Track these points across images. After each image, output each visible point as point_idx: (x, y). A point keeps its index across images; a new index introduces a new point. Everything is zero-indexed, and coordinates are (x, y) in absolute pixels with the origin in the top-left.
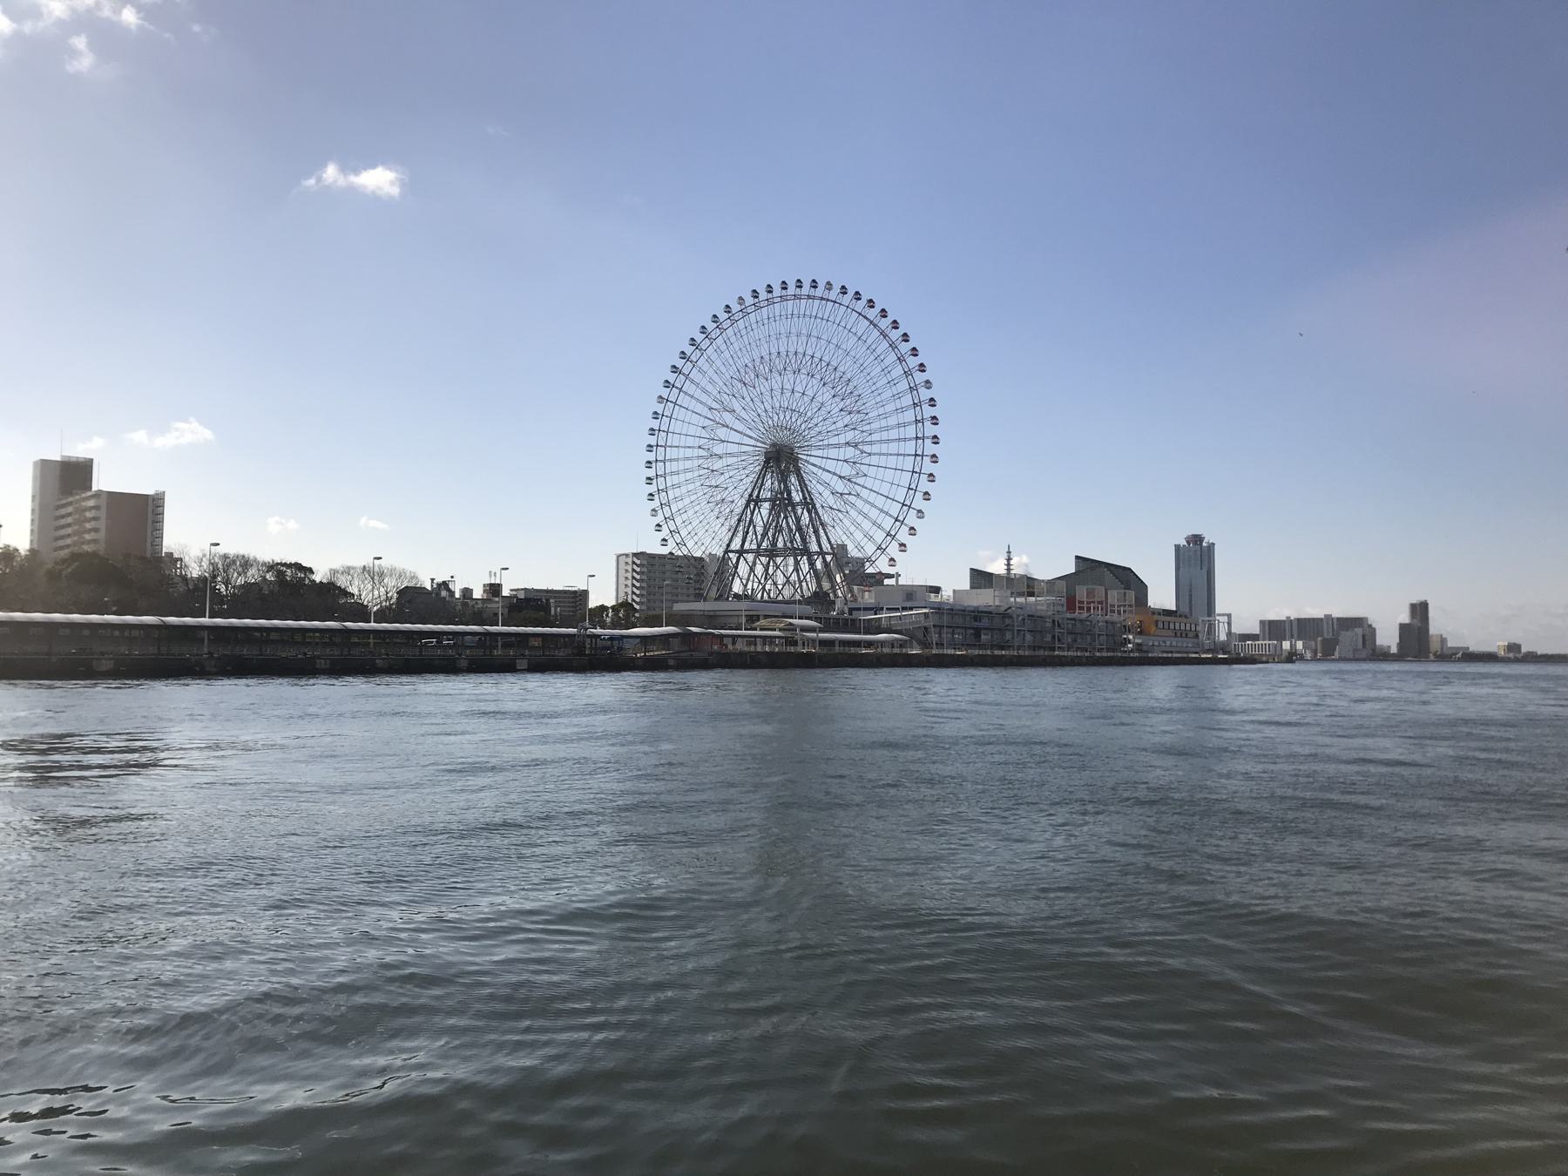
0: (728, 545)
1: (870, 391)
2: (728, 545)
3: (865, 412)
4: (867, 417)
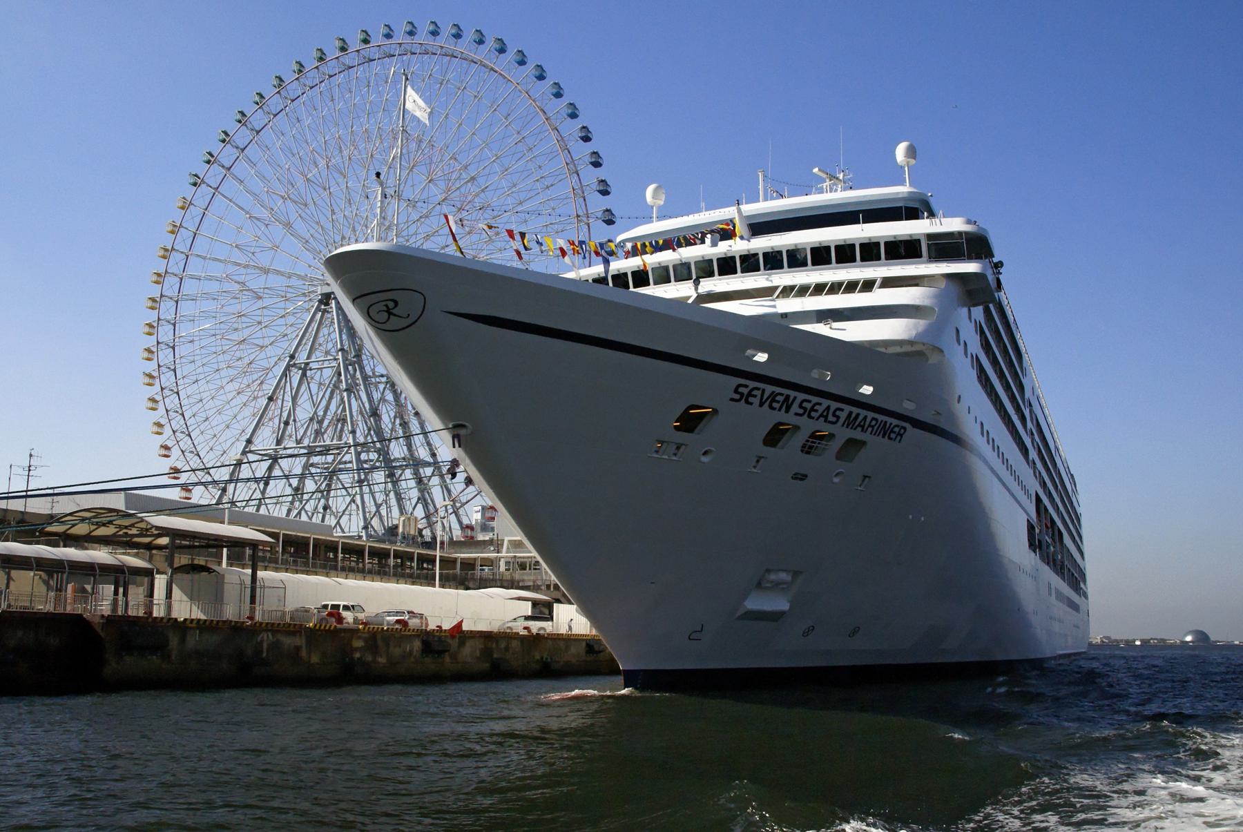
2: (249, 441)
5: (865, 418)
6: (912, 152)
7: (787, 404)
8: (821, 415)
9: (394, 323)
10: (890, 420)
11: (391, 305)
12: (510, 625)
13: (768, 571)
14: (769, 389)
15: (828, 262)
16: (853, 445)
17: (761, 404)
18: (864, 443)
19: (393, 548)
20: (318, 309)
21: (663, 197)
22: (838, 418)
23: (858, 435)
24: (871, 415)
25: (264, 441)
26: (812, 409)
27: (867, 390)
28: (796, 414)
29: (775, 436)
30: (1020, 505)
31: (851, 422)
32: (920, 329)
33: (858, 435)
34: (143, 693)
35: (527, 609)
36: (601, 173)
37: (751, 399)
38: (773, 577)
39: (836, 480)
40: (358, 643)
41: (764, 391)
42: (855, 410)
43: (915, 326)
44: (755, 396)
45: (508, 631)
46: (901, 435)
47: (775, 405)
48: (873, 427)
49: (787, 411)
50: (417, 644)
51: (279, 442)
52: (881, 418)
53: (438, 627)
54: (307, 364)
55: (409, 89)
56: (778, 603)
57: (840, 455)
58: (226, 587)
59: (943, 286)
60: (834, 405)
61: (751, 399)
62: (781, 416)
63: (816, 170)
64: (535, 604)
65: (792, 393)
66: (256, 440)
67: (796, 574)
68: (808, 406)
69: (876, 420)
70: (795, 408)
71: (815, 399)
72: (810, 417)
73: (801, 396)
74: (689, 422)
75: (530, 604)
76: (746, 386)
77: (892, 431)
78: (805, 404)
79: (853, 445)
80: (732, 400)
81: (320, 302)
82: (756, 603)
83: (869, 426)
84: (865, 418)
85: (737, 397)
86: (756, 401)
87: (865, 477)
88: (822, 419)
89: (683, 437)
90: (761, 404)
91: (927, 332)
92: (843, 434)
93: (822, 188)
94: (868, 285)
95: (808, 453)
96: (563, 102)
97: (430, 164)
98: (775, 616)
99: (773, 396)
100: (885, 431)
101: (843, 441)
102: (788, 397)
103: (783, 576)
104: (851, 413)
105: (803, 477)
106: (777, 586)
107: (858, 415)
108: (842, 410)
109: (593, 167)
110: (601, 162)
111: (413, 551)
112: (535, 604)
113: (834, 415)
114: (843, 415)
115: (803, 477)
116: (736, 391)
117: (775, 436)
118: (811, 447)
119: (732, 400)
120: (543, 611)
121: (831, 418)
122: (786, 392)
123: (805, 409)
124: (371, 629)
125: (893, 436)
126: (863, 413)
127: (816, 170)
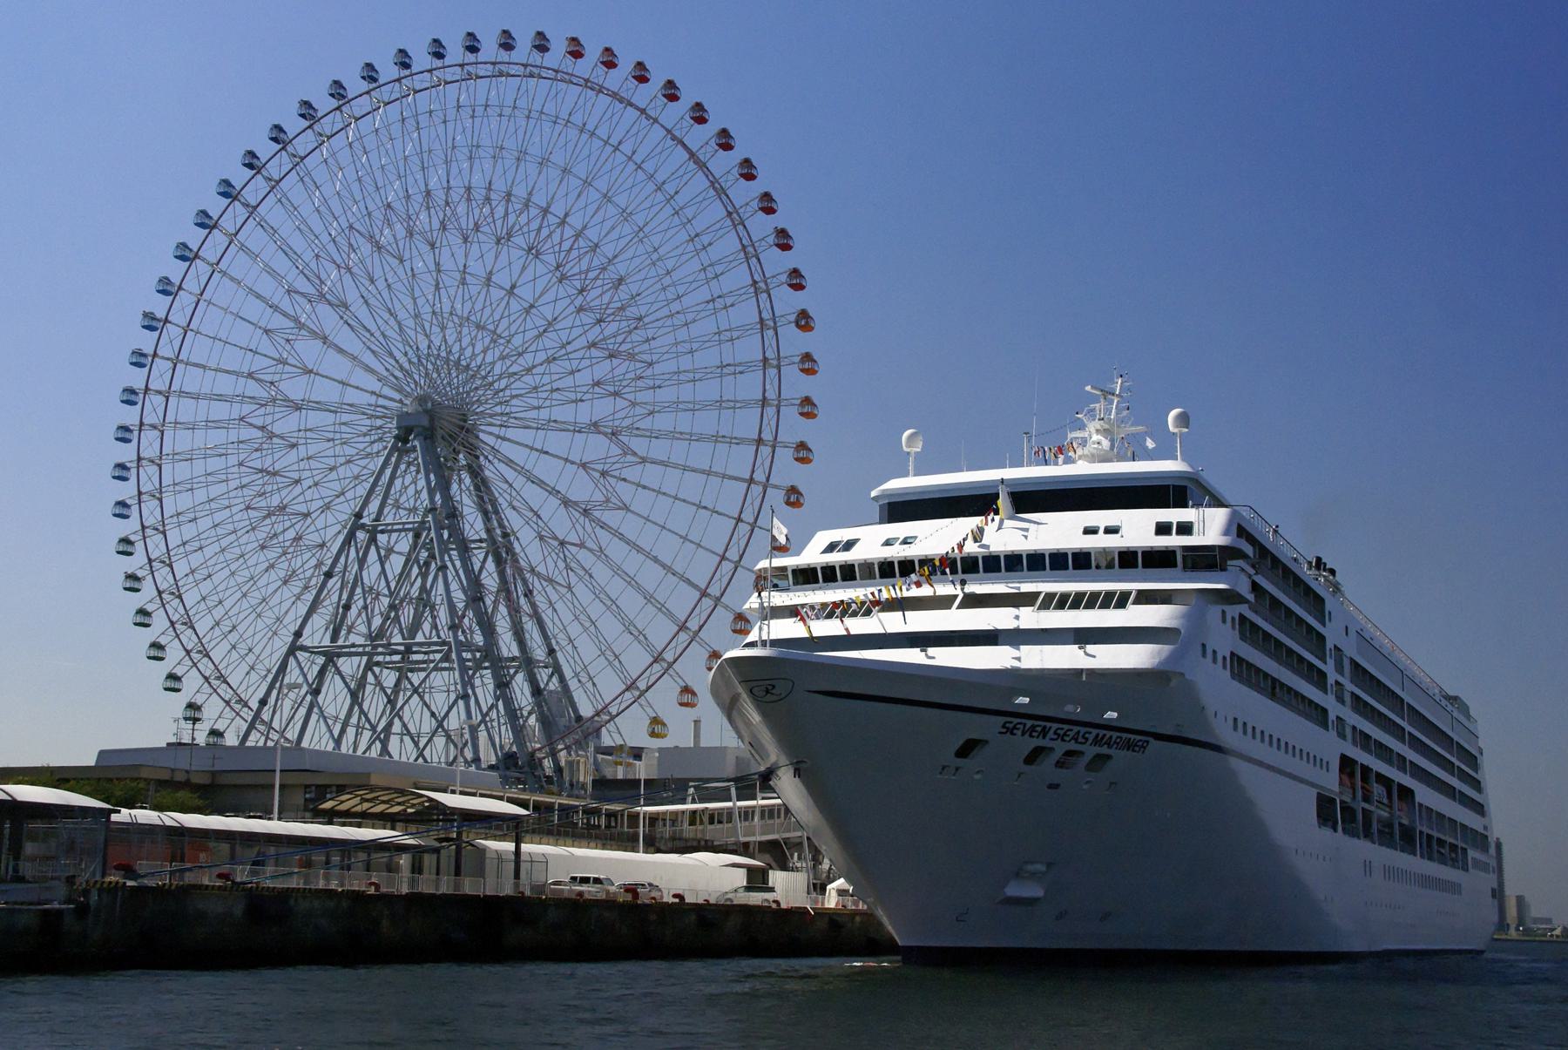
0: (298, 634)
1: (665, 312)
2: (298, 634)
3: (647, 357)
4: (649, 372)
5: (1111, 737)
6: (1183, 420)
7: (1044, 732)
8: (1073, 738)
9: (769, 697)
10: (1132, 737)
11: (770, 688)
12: (730, 896)
13: (1026, 863)
14: (1029, 723)
15: (1135, 566)
16: (1101, 759)
17: (1023, 734)
18: (1109, 757)
19: (558, 801)
20: (394, 448)
21: (920, 444)
22: (1087, 739)
23: (1105, 750)
24: (1115, 734)
25: (316, 634)
26: (1065, 734)
27: (1112, 715)
28: (1052, 739)
29: (1033, 757)
30: (1301, 781)
31: (1097, 741)
32: (1164, 655)
33: (1105, 750)
34: (206, 973)
35: (740, 878)
36: (777, 221)
37: (1015, 731)
38: (1030, 868)
39: (1085, 787)
40: (653, 917)
41: (1025, 725)
42: (1102, 732)
43: (1159, 652)
44: (1018, 729)
45: (729, 903)
46: (1145, 748)
47: (1034, 734)
48: (1118, 744)
49: (1044, 737)
50: (693, 917)
51: (334, 638)
52: (1125, 735)
53: (675, 896)
54: (375, 527)
55: (775, 519)
56: (1033, 890)
57: (1090, 767)
58: (487, 861)
59: (1194, 602)
60: (1083, 730)
61: (1015, 731)
62: (1040, 742)
63: (1088, 388)
64: (751, 871)
65: (1048, 724)
66: (307, 632)
67: (1049, 865)
68: (1061, 732)
69: (1121, 738)
70: (1051, 734)
71: (1066, 727)
72: (1063, 740)
73: (1055, 726)
74: (967, 749)
75: (742, 873)
76: (1011, 722)
77: (1136, 745)
78: (1059, 731)
79: (1101, 759)
80: (1000, 733)
81: (397, 438)
82: (1014, 890)
83: (1115, 742)
84: (1111, 737)
85: (1004, 730)
86: (1019, 733)
87: (1111, 783)
88: (1073, 741)
89: (960, 762)
90: (1023, 734)
91: (1171, 658)
92: (1091, 751)
93: (1093, 410)
94: (1122, 601)
95: (1061, 767)
96: (735, 156)
97: (560, 252)
98: (1031, 902)
99: (1033, 728)
100: (1130, 746)
101: (1092, 756)
102: (1045, 727)
103: (1041, 867)
104: (1097, 735)
105: (1056, 787)
106: (1033, 875)
107: (1105, 735)
108: (1090, 733)
109: (780, 251)
110: (775, 207)
111: (553, 801)
112: (751, 871)
113: (1083, 736)
114: (1091, 737)
115: (1056, 787)
116: (1004, 727)
117: (1033, 757)
118: (1063, 763)
119: (1000, 733)
120: (757, 880)
121: (1080, 740)
122: (1043, 723)
123: (1059, 735)
124: (105, 885)
125: (1137, 749)
126: (1109, 734)
127: (1088, 388)
